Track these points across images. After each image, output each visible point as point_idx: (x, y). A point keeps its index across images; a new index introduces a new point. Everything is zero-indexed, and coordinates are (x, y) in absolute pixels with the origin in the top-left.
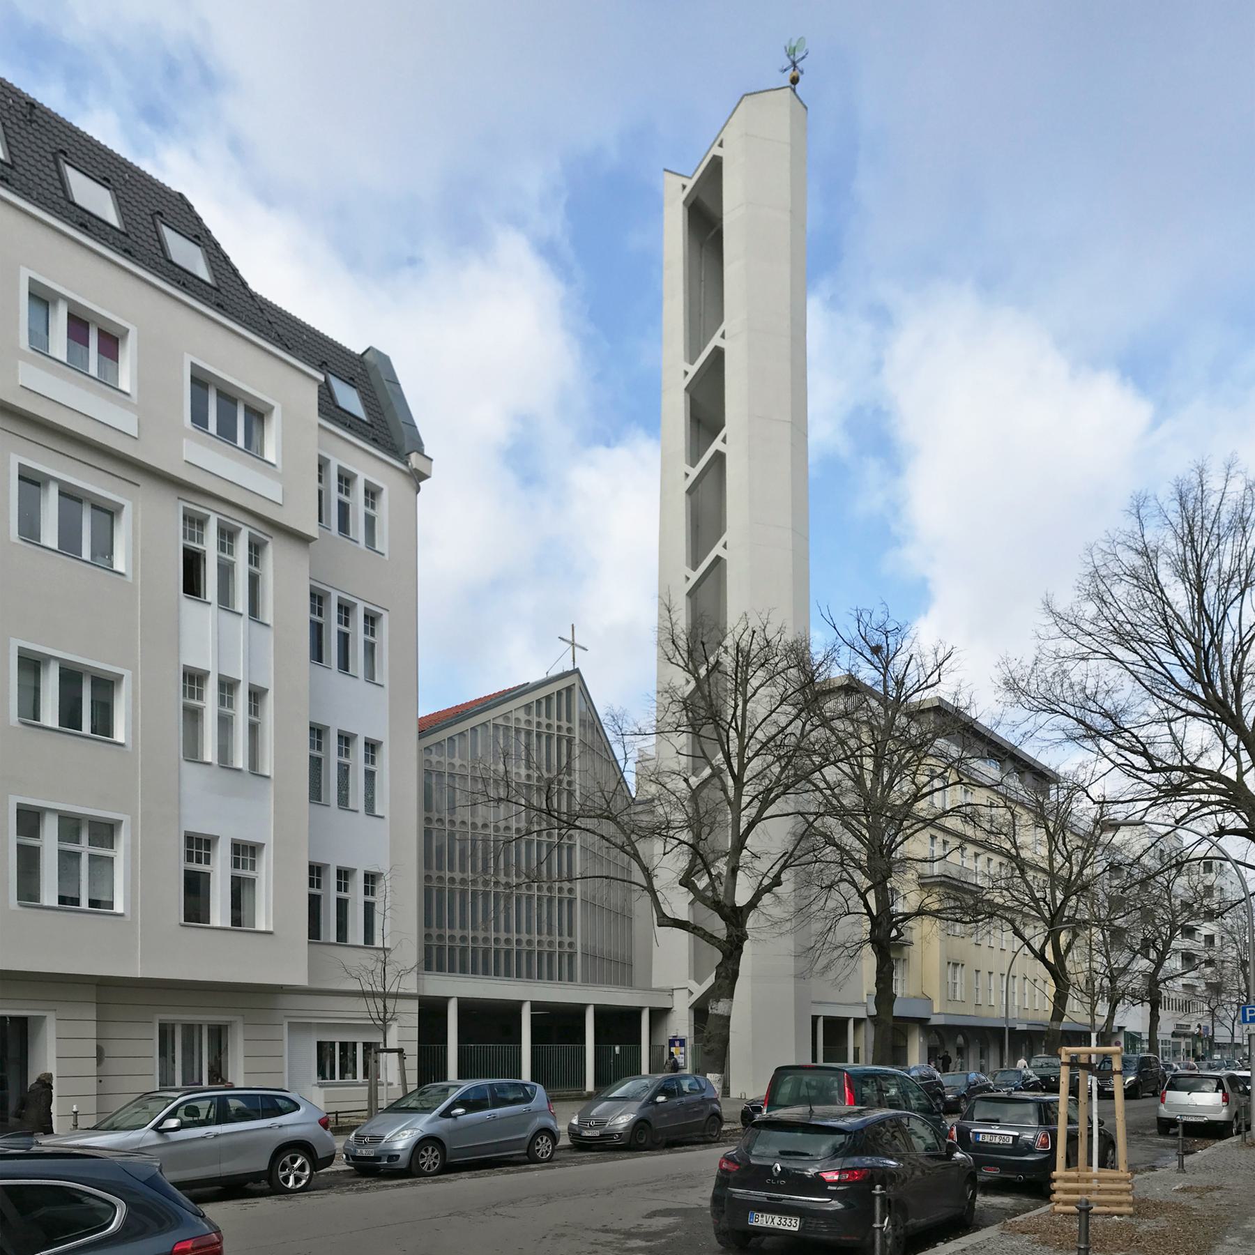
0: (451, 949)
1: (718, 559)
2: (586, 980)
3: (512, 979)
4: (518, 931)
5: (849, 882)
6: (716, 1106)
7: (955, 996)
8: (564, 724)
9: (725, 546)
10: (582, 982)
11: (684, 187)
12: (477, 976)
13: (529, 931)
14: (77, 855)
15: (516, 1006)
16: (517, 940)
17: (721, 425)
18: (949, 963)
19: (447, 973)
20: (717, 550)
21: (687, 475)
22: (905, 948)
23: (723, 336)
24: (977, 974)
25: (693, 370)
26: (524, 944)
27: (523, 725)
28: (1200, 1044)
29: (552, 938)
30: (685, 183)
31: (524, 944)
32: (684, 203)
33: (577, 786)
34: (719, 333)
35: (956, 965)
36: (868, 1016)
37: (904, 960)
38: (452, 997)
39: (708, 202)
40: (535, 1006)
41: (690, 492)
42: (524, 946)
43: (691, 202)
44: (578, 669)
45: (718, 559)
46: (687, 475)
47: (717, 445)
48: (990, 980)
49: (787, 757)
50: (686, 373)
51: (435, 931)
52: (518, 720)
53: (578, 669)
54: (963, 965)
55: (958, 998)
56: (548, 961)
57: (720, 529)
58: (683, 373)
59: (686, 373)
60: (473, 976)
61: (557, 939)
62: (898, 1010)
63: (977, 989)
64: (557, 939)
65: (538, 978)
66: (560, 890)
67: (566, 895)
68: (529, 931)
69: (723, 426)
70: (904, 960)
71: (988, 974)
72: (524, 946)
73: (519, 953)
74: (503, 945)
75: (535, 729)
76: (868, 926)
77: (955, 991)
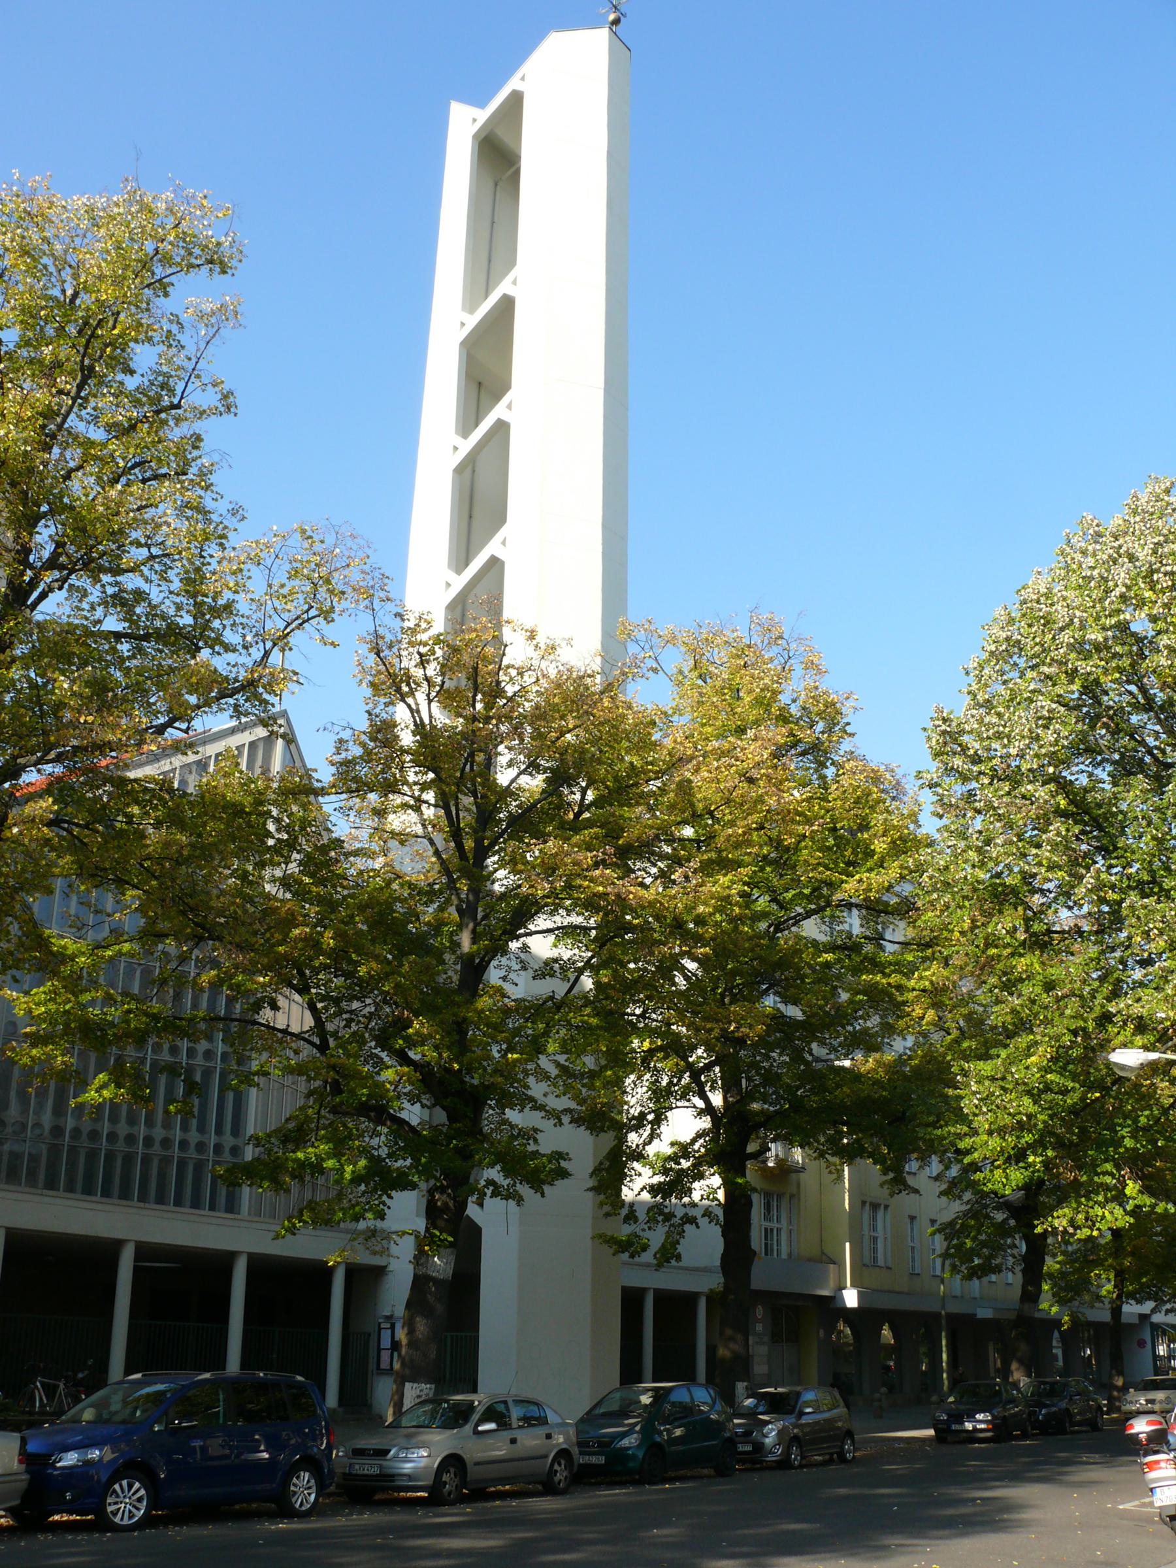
0: (110, 1156)
3: (202, 1212)
4: (219, 1131)
7: (875, 1259)
12: (147, 1205)
15: (113, 1248)
16: (180, 1142)
18: (864, 1203)
20: (493, 548)
22: (794, 1176)
24: (912, 1223)
26: (84, 1137)
28: (425, 1454)
32: (475, 137)
35: (875, 1207)
37: (792, 1196)
39: (502, 134)
40: (145, 1251)
42: (121, 1146)
44: (285, 711)
45: (495, 563)
47: (499, 412)
48: (912, 1229)
49: (62, 567)
53: (285, 711)
54: (886, 1207)
55: (881, 1262)
57: (499, 518)
60: (142, 1205)
61: (213, 1139)
62: (761, 1277)
63: (913, 1248)
64: (213, 1139)
65: (139, 1200)
70: (792, 1196)
71: (908, 1221)
72: (121, 1146)
77: (875, 1251)
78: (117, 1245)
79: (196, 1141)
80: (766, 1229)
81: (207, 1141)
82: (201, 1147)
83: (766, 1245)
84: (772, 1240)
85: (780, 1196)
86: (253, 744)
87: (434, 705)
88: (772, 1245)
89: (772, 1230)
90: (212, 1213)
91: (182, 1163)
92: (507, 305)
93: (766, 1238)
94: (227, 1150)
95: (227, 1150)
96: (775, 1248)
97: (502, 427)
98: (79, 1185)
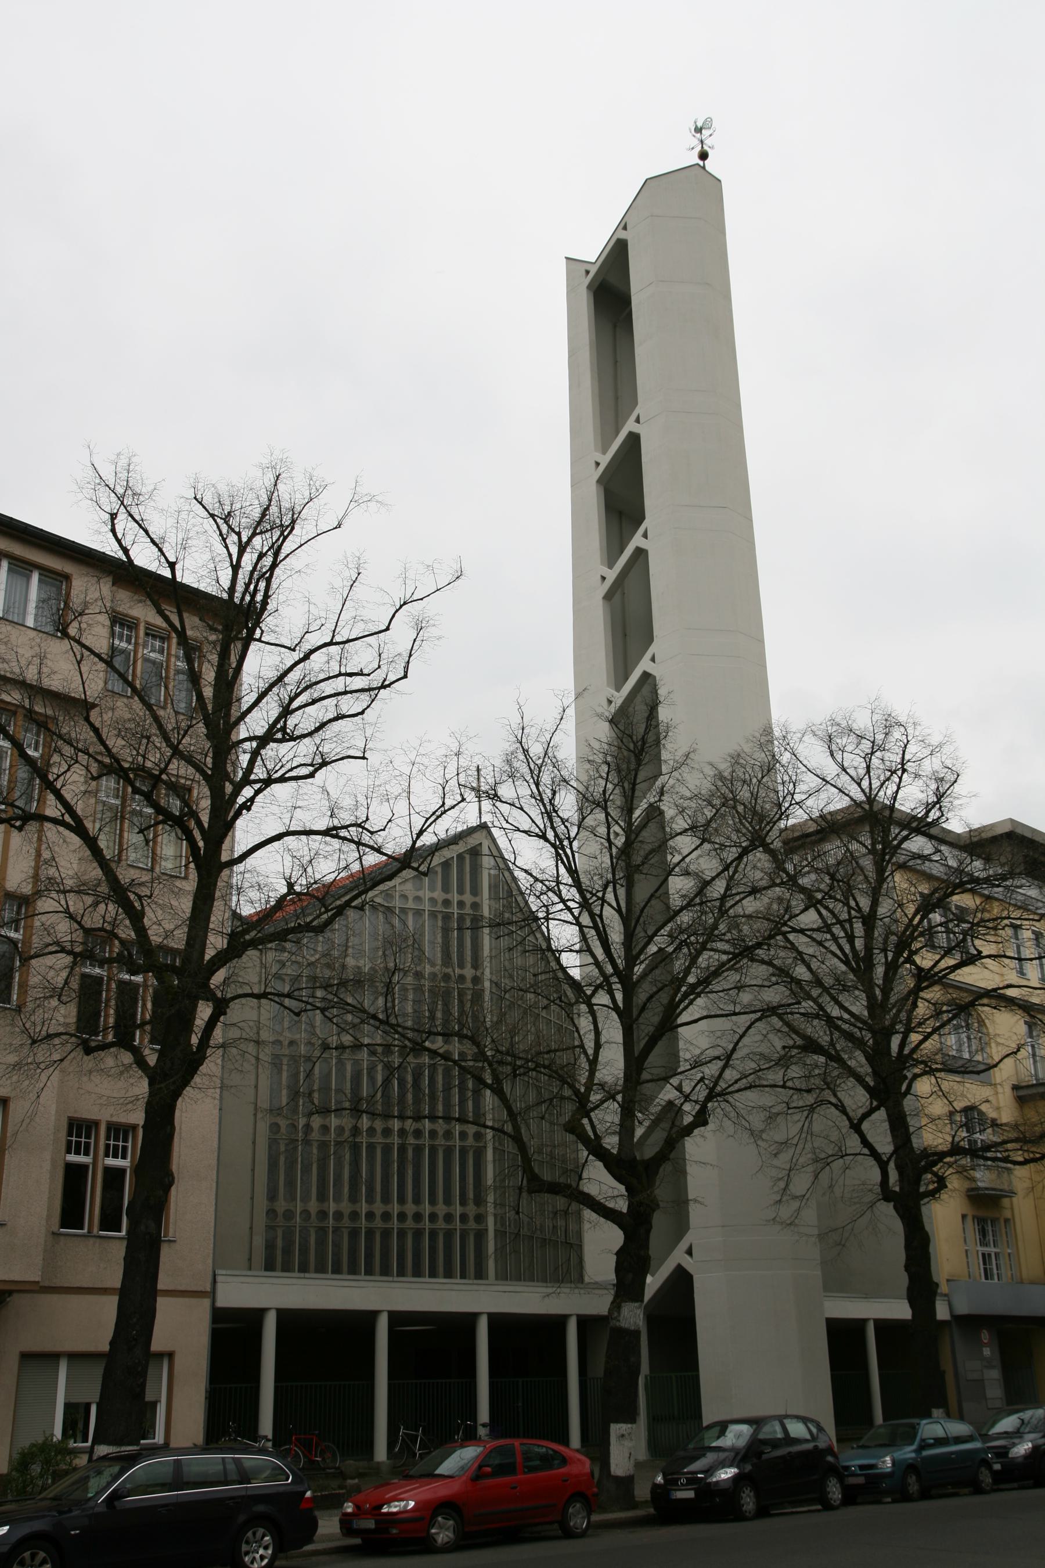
1: (646, 676)
2: (503, 1276)
5: (836, 1106)
6: (830, 1459)
8: (468, 898)
9: (653, 659)
10: (497, 1279)
11: (587, 272)
12: (307, 1275)
13: (448, 1201)
14: (72, 1141)
16: (461, 1216)
17: (642, 518)
19: (363, 1277)
20: (644, 665)
21: (603, 578)
23: (638, 421)
25: (605, 460)
26: (346, 1219)
27: (410, 904)
29: (388, 1208)
30: (588, 269)
31: (346, 1219)
32: (589, 287)
33: (487, 984)
34: (633, 417)
36: (952, 1316)
37: (1007, 1221)
38: (571, 1315)
41: (608, 597)
43: (597, 284)
45: (646, 676)
46: (603, 578)
47: (637, 541)
50: (598, 464)
51: (281, 1206)
52: (404, 897)
53: (485, 822)
56: (475, 1251)
58: (594, 465)
59: (598, 464)
60: (302, 1275)
66: (463, 1135)
67: (440, 1141)
68: (417, 1201)
69: (643, 518)
73: (433, 1234)
74: (378, 1223)
75: (456, 911)
76: (145, 1083)
78: (374, 1314)
79: (444, 1213)
80: (983, 1255)
81: (453, 1212)
82: (449, 1218)
83: (985, 1270)
84: (991, 1264)
85: (994, 1221)
86: (460, 857)
87: (544, 1450)
88: (991, 1269)
89: (989, 1255)
90: (463, 1281)
91: (433, 1234)
92: (634, 440)
93: (985, 1263)
94: (471, 1218)
95: (471, 1218)
96: (995, 1271)
97: (640, 554)
98: (441, 1269)
